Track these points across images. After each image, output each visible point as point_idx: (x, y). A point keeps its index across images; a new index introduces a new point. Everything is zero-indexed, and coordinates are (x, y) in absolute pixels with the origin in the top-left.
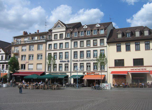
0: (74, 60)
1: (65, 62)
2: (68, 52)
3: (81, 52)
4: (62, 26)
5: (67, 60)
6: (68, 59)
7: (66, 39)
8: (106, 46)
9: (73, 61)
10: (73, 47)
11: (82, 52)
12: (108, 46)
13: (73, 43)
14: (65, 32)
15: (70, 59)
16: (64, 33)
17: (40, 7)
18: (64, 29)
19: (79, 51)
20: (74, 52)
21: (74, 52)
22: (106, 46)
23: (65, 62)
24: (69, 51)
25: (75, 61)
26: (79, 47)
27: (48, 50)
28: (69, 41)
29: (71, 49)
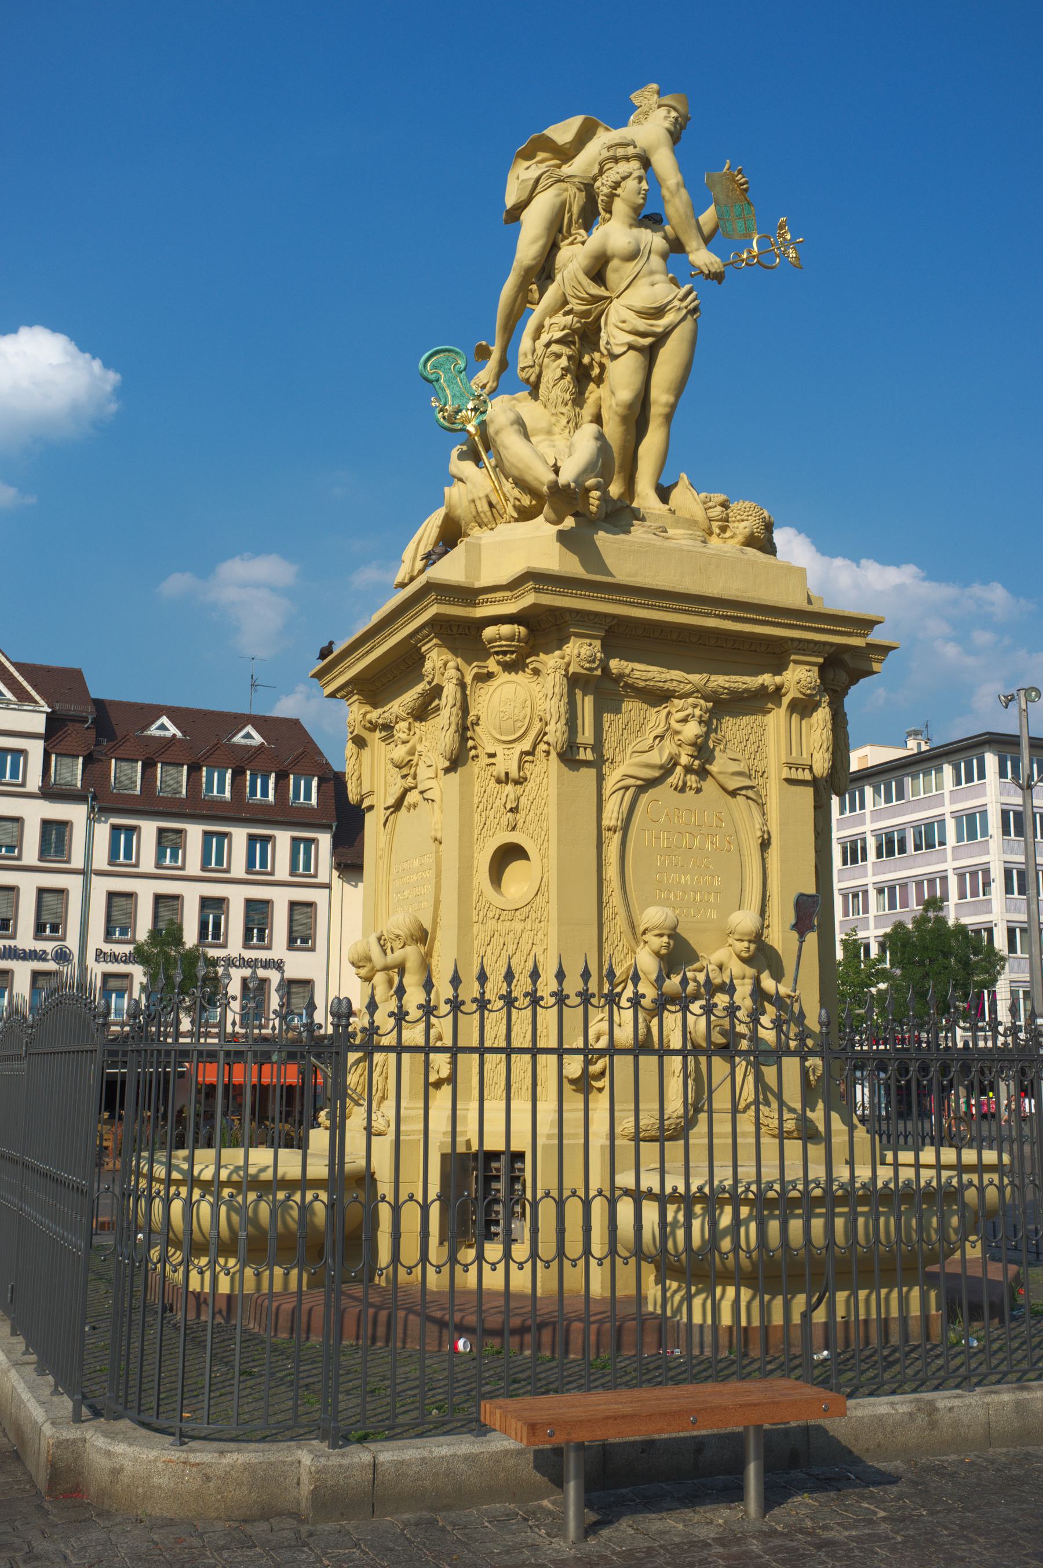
0: (107, 948)
1: (40, 956)
2: (62, 892)
3: (251, 905)
4: (23, 696)
5: (49, 946)
6: (63, 939)
7: (50, 792)
8: (328, 886)
9: (100, 955)
10: (101, 860)
11: (212, 905)
12: (337, 883)
13: (102, 832)
14: (40, 744)
15: (72, 943)
16: (36, 749)
17: (718, 260)
18: (37, 723)
19: (237, 897)
20: (111, 895)
21: (111, 895)
22: (328, 886)
23: (40, 956)
24: (73, 884)
25: (115, 958)
26: (193, 865)
27: (106, 867)
28: (76, 813)
29: (86, 872)
